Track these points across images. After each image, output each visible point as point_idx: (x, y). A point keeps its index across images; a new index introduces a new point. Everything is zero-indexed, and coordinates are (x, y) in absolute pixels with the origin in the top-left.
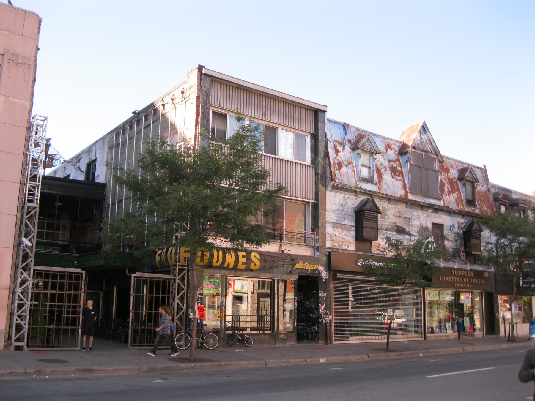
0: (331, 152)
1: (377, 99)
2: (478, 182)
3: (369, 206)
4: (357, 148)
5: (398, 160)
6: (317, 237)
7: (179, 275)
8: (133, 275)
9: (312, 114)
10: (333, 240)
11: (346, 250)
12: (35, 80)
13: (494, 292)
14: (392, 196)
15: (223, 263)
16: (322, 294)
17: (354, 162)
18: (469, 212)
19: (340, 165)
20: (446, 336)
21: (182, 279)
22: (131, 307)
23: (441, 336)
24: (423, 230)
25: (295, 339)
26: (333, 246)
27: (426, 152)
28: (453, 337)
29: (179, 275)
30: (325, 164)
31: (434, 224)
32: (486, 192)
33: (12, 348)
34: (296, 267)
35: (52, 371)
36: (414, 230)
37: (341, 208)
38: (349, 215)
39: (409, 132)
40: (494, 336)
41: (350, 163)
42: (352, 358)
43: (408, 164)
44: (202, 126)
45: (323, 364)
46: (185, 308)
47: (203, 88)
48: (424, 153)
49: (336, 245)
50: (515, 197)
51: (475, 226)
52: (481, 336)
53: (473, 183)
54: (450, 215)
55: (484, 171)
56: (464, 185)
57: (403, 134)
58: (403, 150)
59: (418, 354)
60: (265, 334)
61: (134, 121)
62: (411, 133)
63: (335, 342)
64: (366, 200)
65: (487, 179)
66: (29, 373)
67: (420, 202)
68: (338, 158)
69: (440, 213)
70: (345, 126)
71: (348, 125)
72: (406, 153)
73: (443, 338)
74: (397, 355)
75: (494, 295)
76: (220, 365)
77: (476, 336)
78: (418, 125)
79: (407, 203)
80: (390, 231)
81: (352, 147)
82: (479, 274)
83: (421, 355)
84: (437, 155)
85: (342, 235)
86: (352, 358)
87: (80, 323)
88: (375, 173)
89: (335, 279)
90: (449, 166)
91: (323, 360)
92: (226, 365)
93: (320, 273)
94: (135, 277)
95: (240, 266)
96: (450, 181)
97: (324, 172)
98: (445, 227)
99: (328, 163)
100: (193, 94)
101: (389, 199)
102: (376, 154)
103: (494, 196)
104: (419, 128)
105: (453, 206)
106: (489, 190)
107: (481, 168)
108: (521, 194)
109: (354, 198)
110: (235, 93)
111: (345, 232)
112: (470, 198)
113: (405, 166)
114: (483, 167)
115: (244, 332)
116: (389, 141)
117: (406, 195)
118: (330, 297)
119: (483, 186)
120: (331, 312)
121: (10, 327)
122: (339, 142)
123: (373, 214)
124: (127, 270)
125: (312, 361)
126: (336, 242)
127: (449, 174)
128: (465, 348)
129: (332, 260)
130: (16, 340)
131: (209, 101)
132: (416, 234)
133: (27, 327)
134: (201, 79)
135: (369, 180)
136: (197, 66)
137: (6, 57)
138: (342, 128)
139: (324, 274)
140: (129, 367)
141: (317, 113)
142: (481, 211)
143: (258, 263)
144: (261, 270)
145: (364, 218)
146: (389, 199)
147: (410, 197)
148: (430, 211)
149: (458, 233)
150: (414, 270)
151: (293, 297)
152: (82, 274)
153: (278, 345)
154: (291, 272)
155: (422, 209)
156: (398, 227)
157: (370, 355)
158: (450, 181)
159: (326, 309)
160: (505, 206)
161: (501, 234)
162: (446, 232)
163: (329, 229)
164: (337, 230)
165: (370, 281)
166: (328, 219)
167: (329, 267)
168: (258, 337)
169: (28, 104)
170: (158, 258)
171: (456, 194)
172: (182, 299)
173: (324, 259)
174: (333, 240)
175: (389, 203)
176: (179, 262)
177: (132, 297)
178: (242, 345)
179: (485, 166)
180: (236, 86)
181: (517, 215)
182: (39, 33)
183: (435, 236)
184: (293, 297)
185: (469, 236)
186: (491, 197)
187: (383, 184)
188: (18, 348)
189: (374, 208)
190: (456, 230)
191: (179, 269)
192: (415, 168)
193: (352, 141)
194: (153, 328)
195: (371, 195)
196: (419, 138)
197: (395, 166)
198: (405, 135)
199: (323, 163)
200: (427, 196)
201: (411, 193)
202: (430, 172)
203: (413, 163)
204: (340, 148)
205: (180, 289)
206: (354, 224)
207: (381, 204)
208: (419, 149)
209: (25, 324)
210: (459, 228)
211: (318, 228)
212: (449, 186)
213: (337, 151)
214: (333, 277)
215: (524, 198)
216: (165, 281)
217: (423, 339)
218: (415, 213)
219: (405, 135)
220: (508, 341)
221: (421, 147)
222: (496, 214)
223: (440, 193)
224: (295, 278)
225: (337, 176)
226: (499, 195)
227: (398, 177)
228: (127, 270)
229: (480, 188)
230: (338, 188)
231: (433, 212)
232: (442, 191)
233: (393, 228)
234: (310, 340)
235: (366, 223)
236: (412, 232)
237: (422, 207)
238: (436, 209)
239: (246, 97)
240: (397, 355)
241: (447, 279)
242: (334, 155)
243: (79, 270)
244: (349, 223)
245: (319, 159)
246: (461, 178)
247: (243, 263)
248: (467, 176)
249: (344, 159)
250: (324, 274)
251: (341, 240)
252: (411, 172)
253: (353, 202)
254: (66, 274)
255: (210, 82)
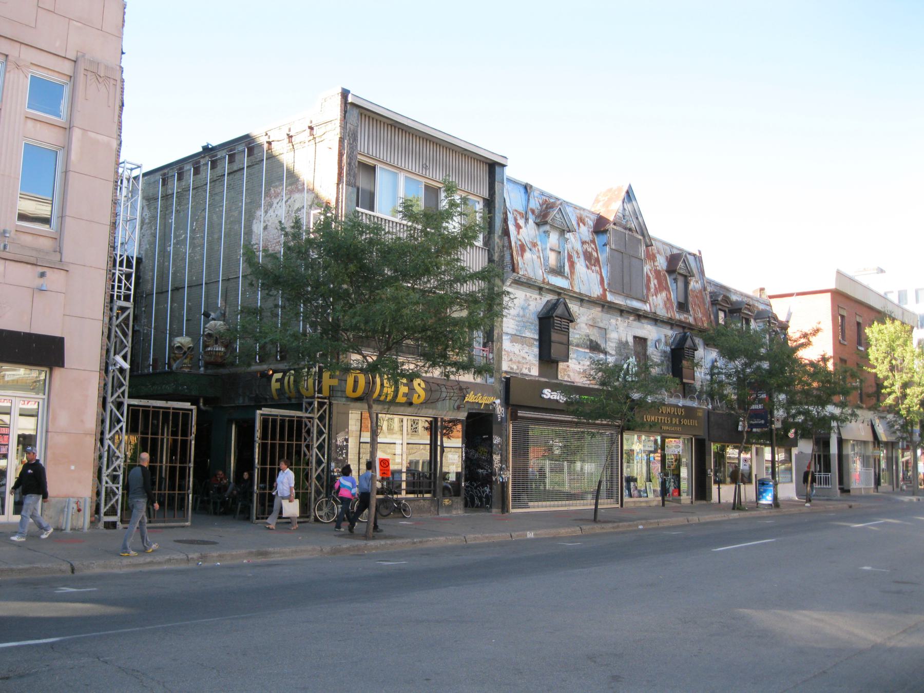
0: (512, 228)
1: (566, 148)
2: (693, 276)
3: (560, 310)
4: (546, 223)
5: (593, 242)
6: (491, 356)
7: (319, 411)
8: (258, 412)
9: (486, 168)
10: (511, 360)
11: (526, 375)
12: (123, 105)
13: (706, 438)
14: (587, 296)
15: (380, 395)
16: (497, 440)
17: (539, 243)
18: (680, 321)
19: (523, 248)
20: (647, 502)
21: (321, 418)
22: (257, 461)
23: (641, 502)
24: (622, 345)
25: (462, 506)
26: (512, 368)
27: (630, 230)
28: (654, 503)
29: (319, 411)
30: (503, 247)
31: (635, 337)
32: (700, 291)
33: (101, 525)
34: (466, 399)
35: (220, 556)
36: (611, 347)
37: (521, 313)
38: (532, 323)
39: (606, 199)
40: (704, 502)
41: (535, 245)
42: (563, 531)
43: (608, 248)
44: (348, 184)
45: (531, 540)
46: (325, 461)
47: (348, 125)
48: (627, 232)
49: (515, 367)
50: (734, 298)
51: (689, 343)
52: (689, 502)
53: (685, 277)
54: (656, 324)
55: (698, 259)
56: (675, 280)
57: (597, 201)
58: (600, 226)
59: (637, 526)
60: (424, 499)
61: (203, 162)
62: (610, 201)
63: (512, 511)
64: (554, 302)
65: (702, 272)
66: (192, 559)
67: (621, 305)
68: (520, 237)
69: (643, 321)
70: (527, 188)
71: (531, 187)
72: (605, 231)
73: (643, 504)
74: (613, 528)
75: (707, 442)
76: (414, 543)
77: (682, 502)
78: (620, 189)
79: (603, 306)
80: (582, 347)
81: (538, 221)
82: (689, 412)
83: (641, 527)
84: (643, 235)
85: (523, 354)
86: (563, 531)
87: (191, 486)
88: (566, 260)
89: (514, 417)
90: (655, 251)
91: (530, 535)
92: (421, 542)
93: (494, 409)
94: (262, 415)
95: (401, 399)
96: (657, 273)
97: (502, 257)
98: (649, 343)
99: (507, 244)
100: (332, 135)
101: (582, 300)
102: (569, 231)
103: (711, 297)
104: (623, 194)
105: (662, 312)
106: (705, 289)
107: (694, 255)
108: (742, 294)
109: (538, 297)
110: (386, 134)
111: (526, 349)
112: (682, 300)
113: (602, 251)
114: (698, 254)
115: (399, 496)
116: (582, 212)
117: (604, 295)
118: (507, 445)
119: (697, 282)
120: (507, 467)
121: (98, 494)
122: (520, 213)
123: (564, 322)
124: (201, 401)
125: (475, 539)
126: (515, 363)
127: (656, 264)
128: (690, 518)
129: (512, 390)
130: (106, 514)
131: (356, 146)
132: (613, 353)
133: (120, 492)
134: (346, 112)
135: (558, 271)
136: (340, 91)
137: (82, 66)
138: (523, 191)
139: (500, 411)
140: (310, 548)
141: (493, 167)
142: (695, 319)
143: (422, 393)
144: (427, 403)
145: (551, 328)
146: (582, 300)
147: (610, 297)
148: (631, 318)
149: (665, 352)
150: (612, 407)
151: (460, 445)
152: (191, 410)
153: (441, 515)
154: (459, 408)
155: (621, 315)
156: (591, 341)
157: (584, 527)
158: (657, 273)
159: (501, 462)
160: (725, 311)
161: (730, 353)
162: (651, 350)
163: (507, 344)
164: (516, 345)
165: (561, 421)
166: (505, 329)
167: (507, 402)
168: (416, 503)
169: (115, 144)
170: (275, 385)
171: (664, 294)
172: (320, 448)
173: (499, 387)
174: (511, 360)
175: (581, 306)
176: (320, 391)
177: (257, 445)
178: (396, 515)
179: (700, 253)
180: (390, 122)
181: (739, 325)
182: (123, 25)
183: (637, 355)
184: (460, 445)
185: (679, 356)
186: (708, 299)
187: (575, 277)
188: (112, 525)
189: (566, 313)
190: (662, 347)
191: (319, 402)
192: (616, 253)
193: (536, 211)
194: (267, 491)
195: (559, 294)
196: (621, 208)
197: (590, 250)
198: (601, 203)
199: (501, 244)
200: (629, 296)
201: (610, 291)
202: (634, 260)
203: (613, 247)
204: (521, 222)
205: (320, 433)
206: (537, 337)
207: (574, 307)
208: (620, 225)
209: (118, 488)
210: (666, 344)
211: (493, 342)
212: (656, 282)
213: (518, 227)
214: (511, 415)
215: (745, 299)
216: (300, 420)
217: (619, 506)
218: (613, 321)
219: (601, 203)
220: (734, 509)
221: (624, 222)
222: (714, 324)
223: (645, 291)
224: (463, 415)
225: (520, 266)
226: (718, 296)
227: (593, 268)
228: (201, 401)
229: (694, 285)
230: (518, 282)
231: (634, 320)
232: (648, 289)
233: (586, 344)
234: (477, 507)
235: (555, 336)
236: (609, 350)
237: (622, 312)
238: (639, 316)
239: (400, 140)
240: (613, 528)
241: (653, 418)
242: (515, 233)
243: (187, 405)
244: (532, 336)
245: (496, 237)
246: (671, 270)
247: (405, 395)
248: (679, 267)
249: (527, 239)
250: (500, 411)
251: (521, 360)
252: (609, 260)
253: (536, 303)
254: (171, 411)
255: (358, 116)
